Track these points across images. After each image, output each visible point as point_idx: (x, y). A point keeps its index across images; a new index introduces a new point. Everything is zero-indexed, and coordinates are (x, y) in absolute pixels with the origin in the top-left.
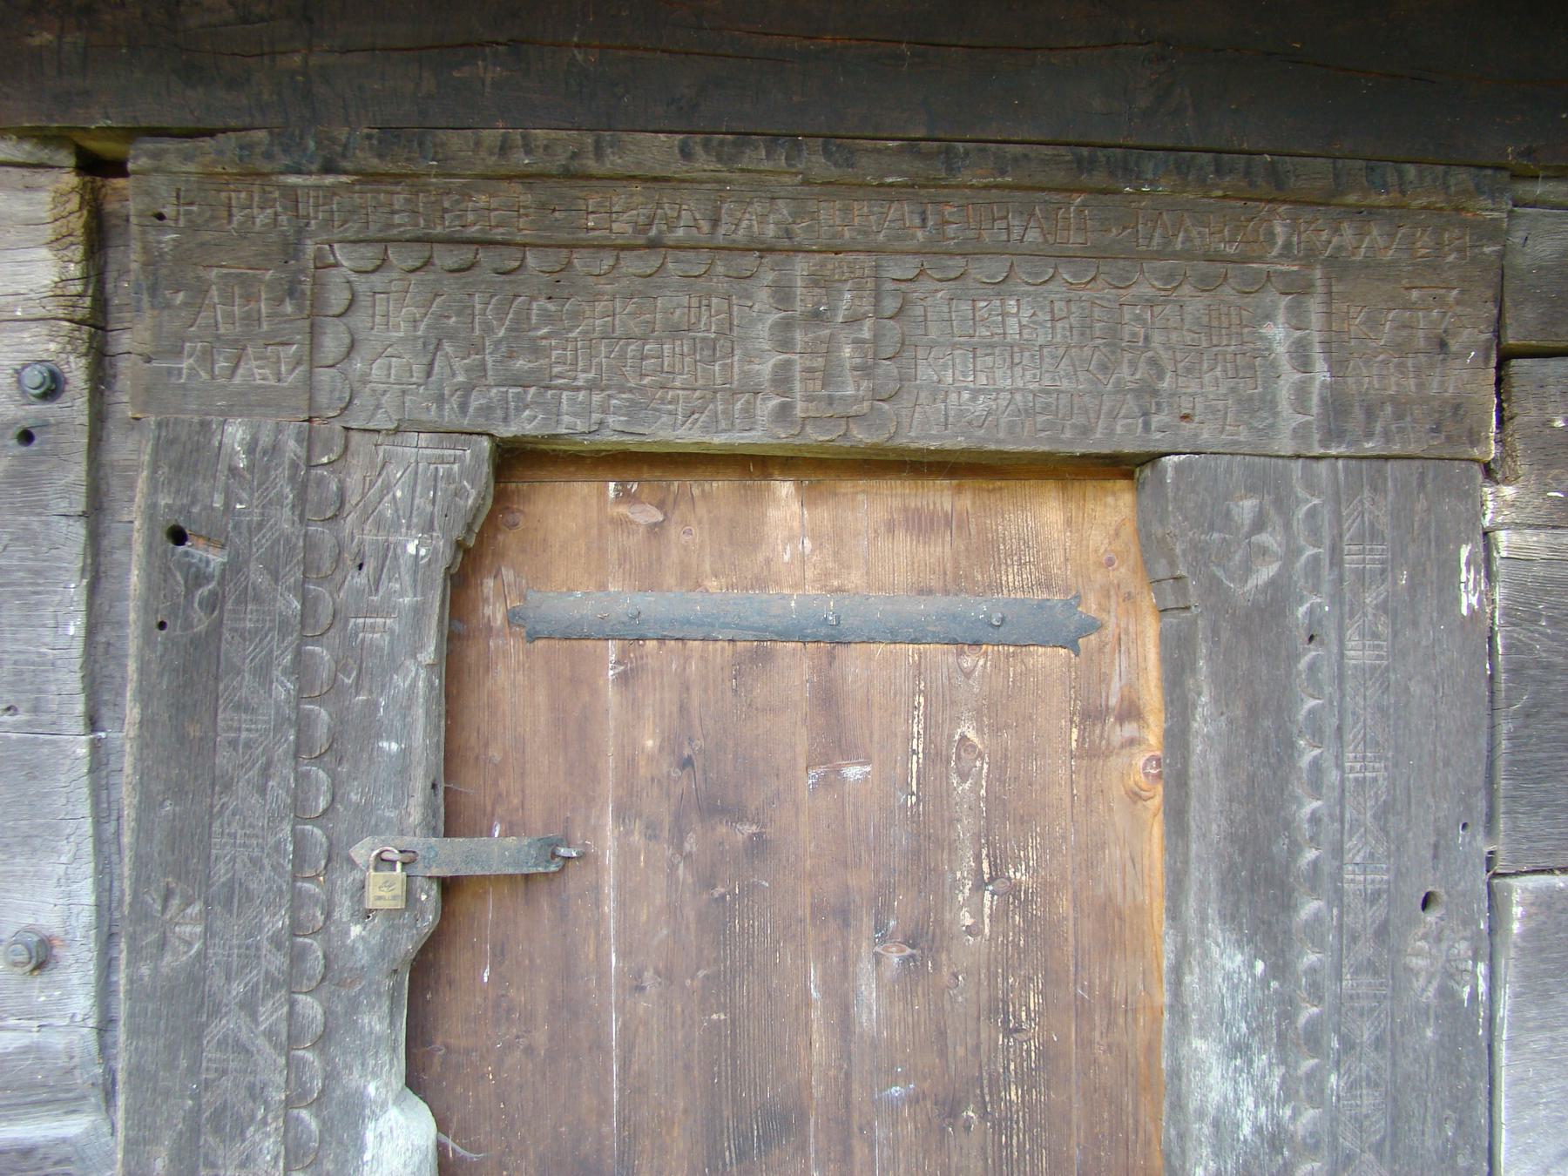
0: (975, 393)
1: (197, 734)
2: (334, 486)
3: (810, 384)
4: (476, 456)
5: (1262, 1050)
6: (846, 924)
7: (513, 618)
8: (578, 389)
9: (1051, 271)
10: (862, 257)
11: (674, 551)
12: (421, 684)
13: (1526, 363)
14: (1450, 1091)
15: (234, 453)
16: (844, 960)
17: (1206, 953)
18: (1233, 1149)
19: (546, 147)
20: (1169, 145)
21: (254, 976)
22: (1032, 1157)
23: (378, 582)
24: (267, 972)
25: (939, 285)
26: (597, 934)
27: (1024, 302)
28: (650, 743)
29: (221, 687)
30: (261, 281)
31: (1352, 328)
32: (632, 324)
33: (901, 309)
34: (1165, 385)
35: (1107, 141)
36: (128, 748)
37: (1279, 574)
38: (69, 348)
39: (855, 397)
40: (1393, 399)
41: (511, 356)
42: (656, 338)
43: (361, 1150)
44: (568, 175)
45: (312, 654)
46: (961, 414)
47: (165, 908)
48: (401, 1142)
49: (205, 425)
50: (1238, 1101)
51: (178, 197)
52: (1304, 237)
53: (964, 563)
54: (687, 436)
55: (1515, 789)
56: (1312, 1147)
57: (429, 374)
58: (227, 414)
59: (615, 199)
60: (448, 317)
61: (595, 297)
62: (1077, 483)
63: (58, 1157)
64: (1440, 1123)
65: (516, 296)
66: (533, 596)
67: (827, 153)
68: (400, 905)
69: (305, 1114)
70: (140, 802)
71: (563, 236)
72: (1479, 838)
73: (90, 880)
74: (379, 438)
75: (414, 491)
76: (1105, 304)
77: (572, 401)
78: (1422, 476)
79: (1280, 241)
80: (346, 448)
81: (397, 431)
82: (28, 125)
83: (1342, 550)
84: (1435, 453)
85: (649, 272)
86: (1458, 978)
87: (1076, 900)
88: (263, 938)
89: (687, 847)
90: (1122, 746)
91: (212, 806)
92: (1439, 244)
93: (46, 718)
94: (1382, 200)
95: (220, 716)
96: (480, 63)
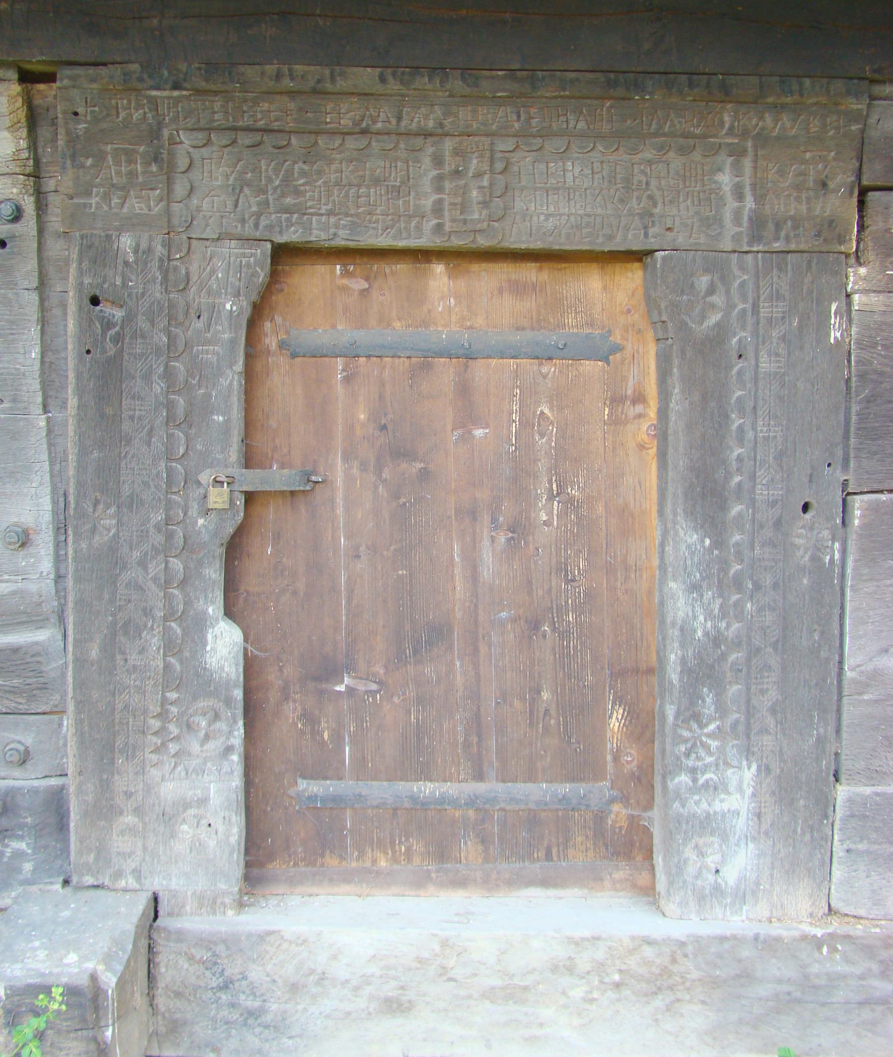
0: (548, 216)
2: (184, 272)
3: (453, 212)
4: (263, 253)
6: (475, 519)
7: (282, 345)
8: (322, 215)
9: (592, 145)
10: (483, 139)
13: (877, 194)
16: (474, 540)
17: (676, 534)
18: (692, 644)
19: (303, 77)
20: (662, 71)
22: (581, 654)
25: (527, 154)
26: (333, 525)
27: (576, 163)
28: (362, 416)
29: (124, 386)
31: (769, 176)
32: (352, 177)
34: (657, 211)
35: (625, 69)
38: (24, 191)
40: (792, 218)
41: (283, 195)
43: (205, 644)
44: (315, 92)
45: (174, 367)
47: (94, 511)
48: (227, 640)
49: (108, 237)
50: (695, 617)
51: (86, 102)
52: (741, 123)
54: (383, 241)
55: (861, 444)
57: (236, 206)
58: (120, 230)
59: (342, 105)
60: (247, 173)
61: (331, 161)
62: (610, 265)
63: (32, 653)
65: (285, 161)
67: (464, 79)
68: (227, 506)
69: (173, 624)
70: (79, 451)
71: (312, 127)
72: (838, 472)
73: (49, 497)
74: (208, 243)
75: (228, 273)
76: (623, 164)
77: (319, 222)
78: (809, 263)
79: (727, 126)
81: (218, 239)
83: (759, 306)
84: (816, 249)
85: (361, 147)
86: (823, 551)
89: (384, 475)
90: (634, 418)
91: (120, 453)
92: (824, 126)
93: (21, 405)
94: (789, 100)
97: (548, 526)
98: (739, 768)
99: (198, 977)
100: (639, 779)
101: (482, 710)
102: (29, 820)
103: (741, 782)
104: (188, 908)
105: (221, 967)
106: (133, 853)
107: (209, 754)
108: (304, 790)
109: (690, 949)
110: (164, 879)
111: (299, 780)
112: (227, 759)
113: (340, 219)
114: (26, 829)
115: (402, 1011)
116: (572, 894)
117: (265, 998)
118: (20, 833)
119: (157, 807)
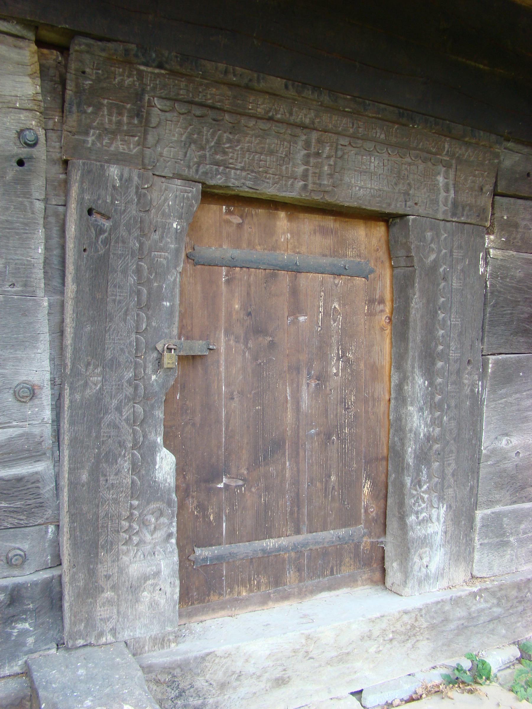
0: (360, 188)
1: (100, 297)
5: (426, 410)
8: (237, 169)
10: (333, 135)
11: (246, 235)
12: (178, 280)
15: (114, 180)
16: (298, 386)
17: (414, 379)
19: (241, 75)
21: (121, 396)
24: (126, 395)
25: (353, 149)
26: (218, 379)
28: (237, 306)
29: (109, 278)
30: (126, 108)
34: (411, 192)
37: (436, 257)
41: (216, 153)
42: (265, 154)
43: (155, 464)
44: (247, 88)
46: (356, 194)
47: (86, 370)
50: (420, 426)
59: (259, 99)
60: (194, 135)
63: (33, 481)
71: (240, 110)
77: (235, 173)
79: (446, 150)
82: (29, 18)
89: (249, 345)
90: (379, 312)
91: (106, 327)
93: (31, 289)
94: (474, 141)
95: (109, 290)
97: (337, 376)
98: (438, 508)
99: (163, 694)
100: (376, 521)
101: (300, 490)
102: (31, 606)
103: (438, 515)
104: (146, 648)
105: (177, 683)
106: (111, 617)
107: (157, 541)
108: (200, 555)
109: (423, 612)
110: (131, 631)
111: (196, 549)
112: (168, 543)
113: (248, 174)
114: (28, 613)
115: (285, 684)
116: (342, 592)
117: (205, 696)
118: (24, 616)
119: (127, 583)
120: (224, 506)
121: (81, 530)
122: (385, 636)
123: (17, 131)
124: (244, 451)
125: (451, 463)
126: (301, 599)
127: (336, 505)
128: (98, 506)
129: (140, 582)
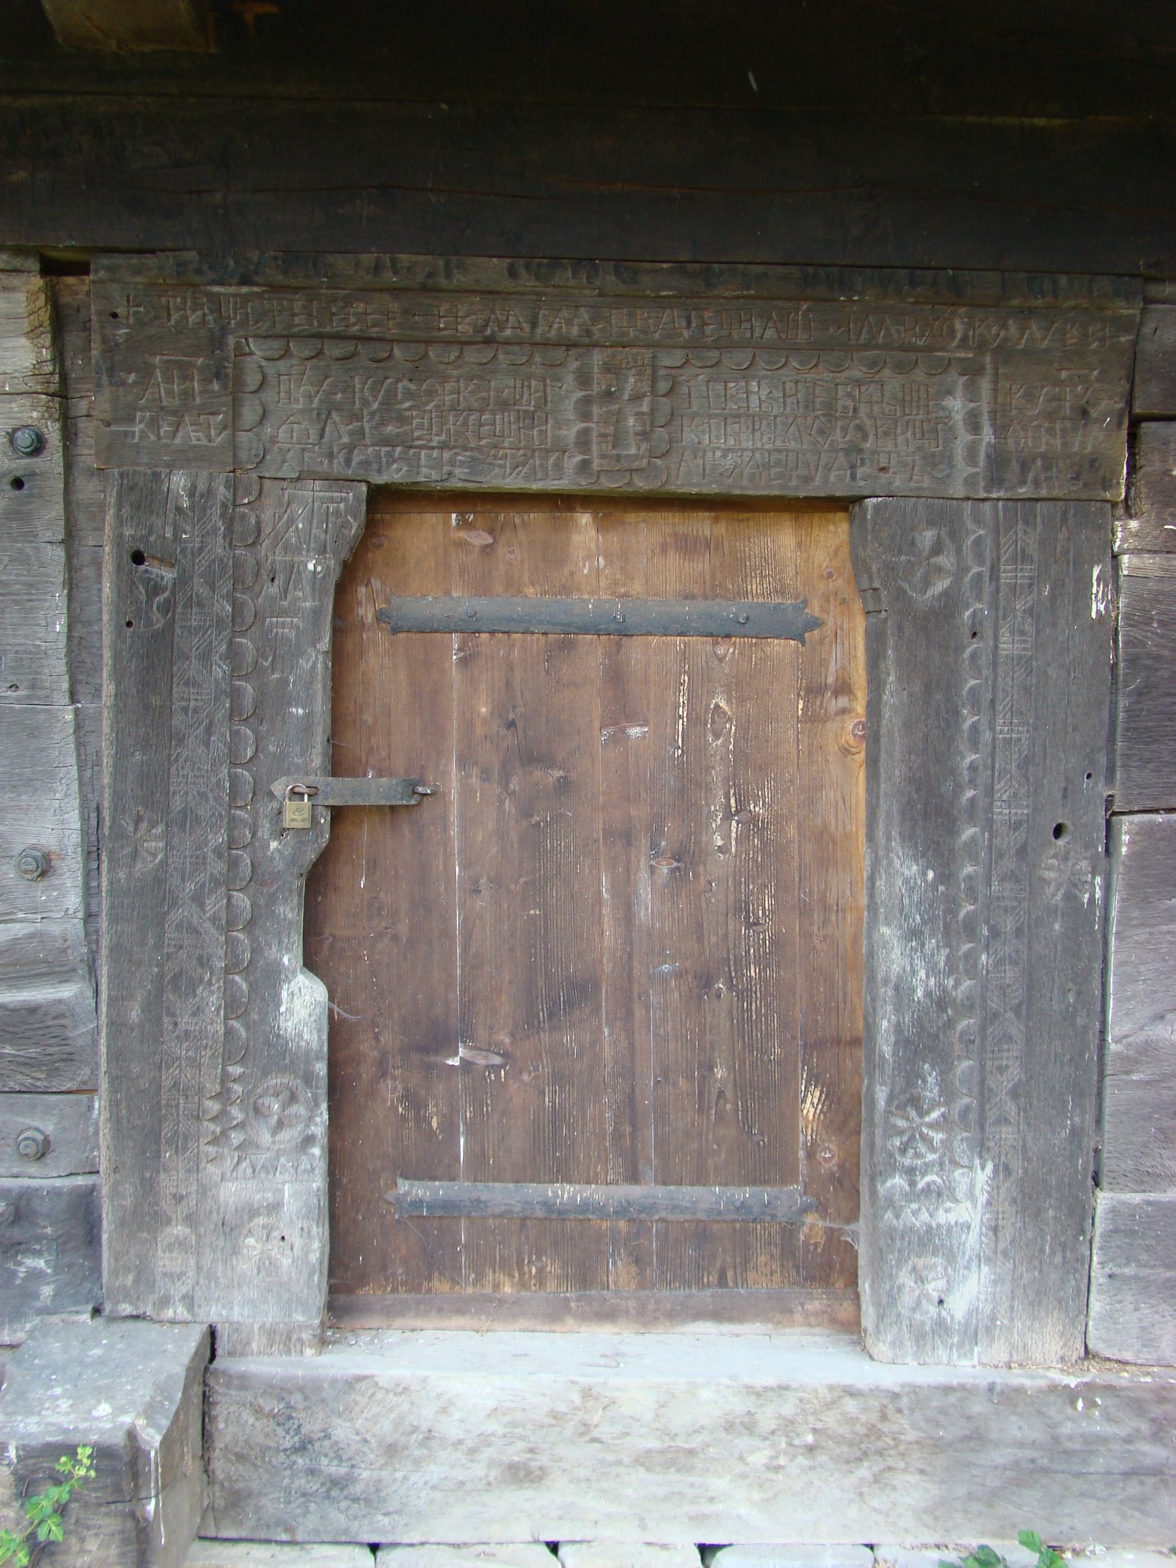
2: (253, 521)
3: (604, 446)
6: (629, 844)
7: (380, 617)
8: (433, 448)
9: (783, 360)
10: (643, 351)
13: (1153, 425)
14: (1072, 969)
15: (179, 496)
16: (628, 871)
17: (890, 864)
18: (909, 1005)
19: (409, 269)
20: (875, 263)
21: (202, 877)
22: (766, 1019)
23: (286, 591)
25: (700, 371)
26: (445, 850)
27: (763, 383)
28: (484, 710)
29: (175, 668)
33: (671, 389)
36: (106, 714)
37: (950, 588)
38: (46, 415)
39: (637, 455)
40: (1043, 456)
41: (383, 423)
43: (278, 1004)
44: (425, 288)
45: (241, 644)
47: (136, 830)
48: (307, 998)
49: (156, 476)
50: (914, 972)
51: (128, 301)
52: (977, 332)
53: (719, 575)
54: (513, 483)
55: (1130, 749)
56: (968, 1007)
57: (322, 436)
58: (171, 466)
60: (336, 394)
61: (444, 379)
64: (1064, 992)
65: (386, 378)
66: (395, 600)
67: (617, 273)
68: (307, 825)
69: (237, 978)
72: (1100, 785)
74: (285, 484)
75: (311, 523)
77: (429, 457)
79: (959, 336)
80: (260, 495)
81: (298, 479)
83: (999, 570)
84: (1074, 496)
87: (799, 828)
88: (208, 850)
89: (512, 786)
90: (837, 714)
91: (170, 755)
93: (41, 693)
94: (1039, 302)
95: (174, 691)
96: (358, 202)
98: (971, 1168)
99: (267, 1435)
100: (840, 1181)
101: (637, 1091)
103: (972, 1186)
104: (254, 1346)
105: (296, 1422)
106: (183, 1274)
108: (406, 1194)
109: (905, 1402)
110: (224, 1307)
111: (400, 1181)
113: (456, 454)
115: (532, 1481)
119: (215, 1214)
120: (461, 1102)
121: (129, 1107)
122: (792, 1434)
123: (8, 433)
124: (504, 997)
125: (1007, 1067)
126: (645, 1325)
127: (730, 1132)
128: (160, 1067)
129: (241, 1217)
